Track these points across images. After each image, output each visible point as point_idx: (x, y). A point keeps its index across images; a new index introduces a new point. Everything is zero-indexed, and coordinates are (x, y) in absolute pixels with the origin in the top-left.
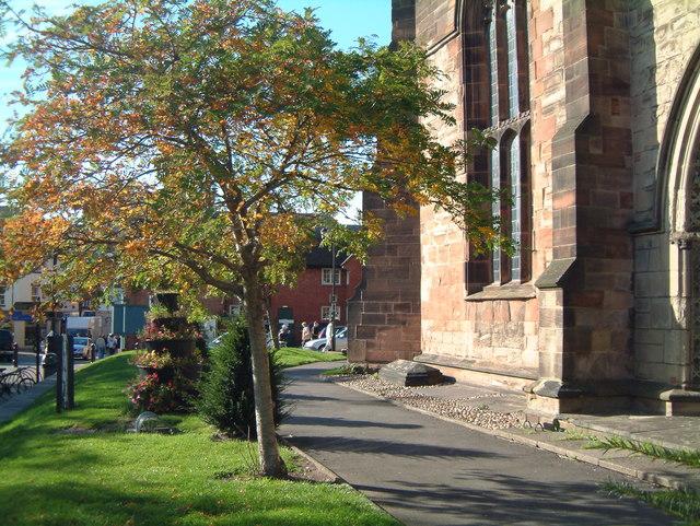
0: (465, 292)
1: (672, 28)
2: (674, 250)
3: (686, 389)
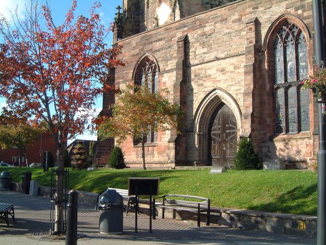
0: (133, 145)
2: (196, 135)
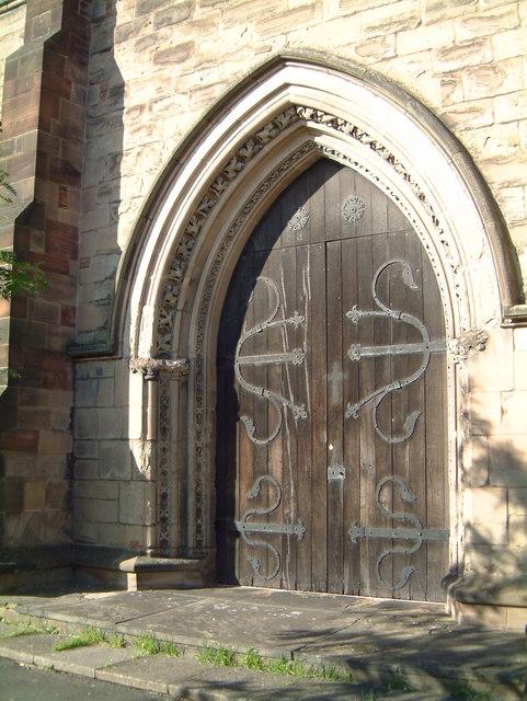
1: (150, 109)
2: (135, 383)
3: (153, 555)
